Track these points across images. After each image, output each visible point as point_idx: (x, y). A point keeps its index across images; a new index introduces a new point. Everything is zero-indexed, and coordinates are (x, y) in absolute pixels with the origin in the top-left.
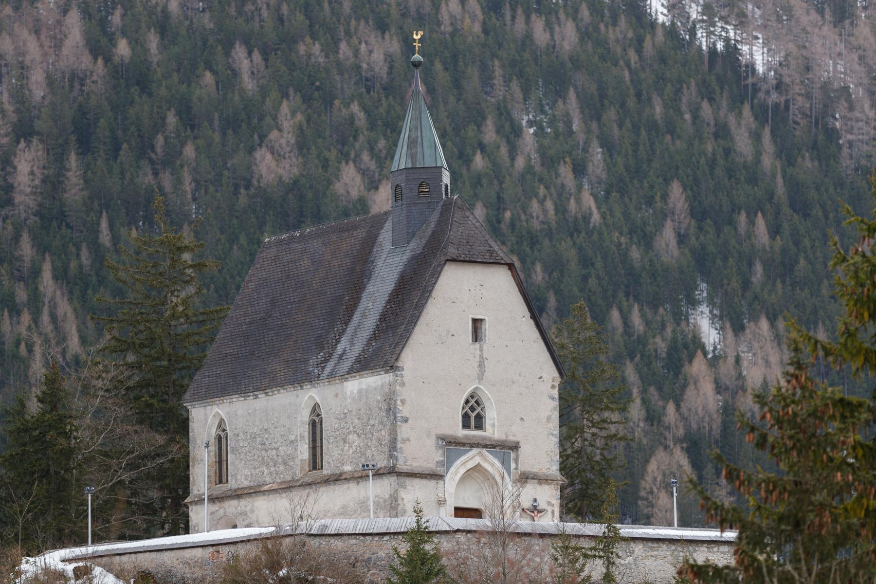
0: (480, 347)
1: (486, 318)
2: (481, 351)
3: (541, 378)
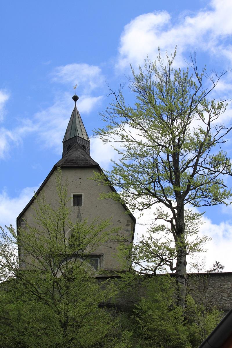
0: (78, 208)
1: (83, 194)
2: (79, 209)
3: (119, 221)
